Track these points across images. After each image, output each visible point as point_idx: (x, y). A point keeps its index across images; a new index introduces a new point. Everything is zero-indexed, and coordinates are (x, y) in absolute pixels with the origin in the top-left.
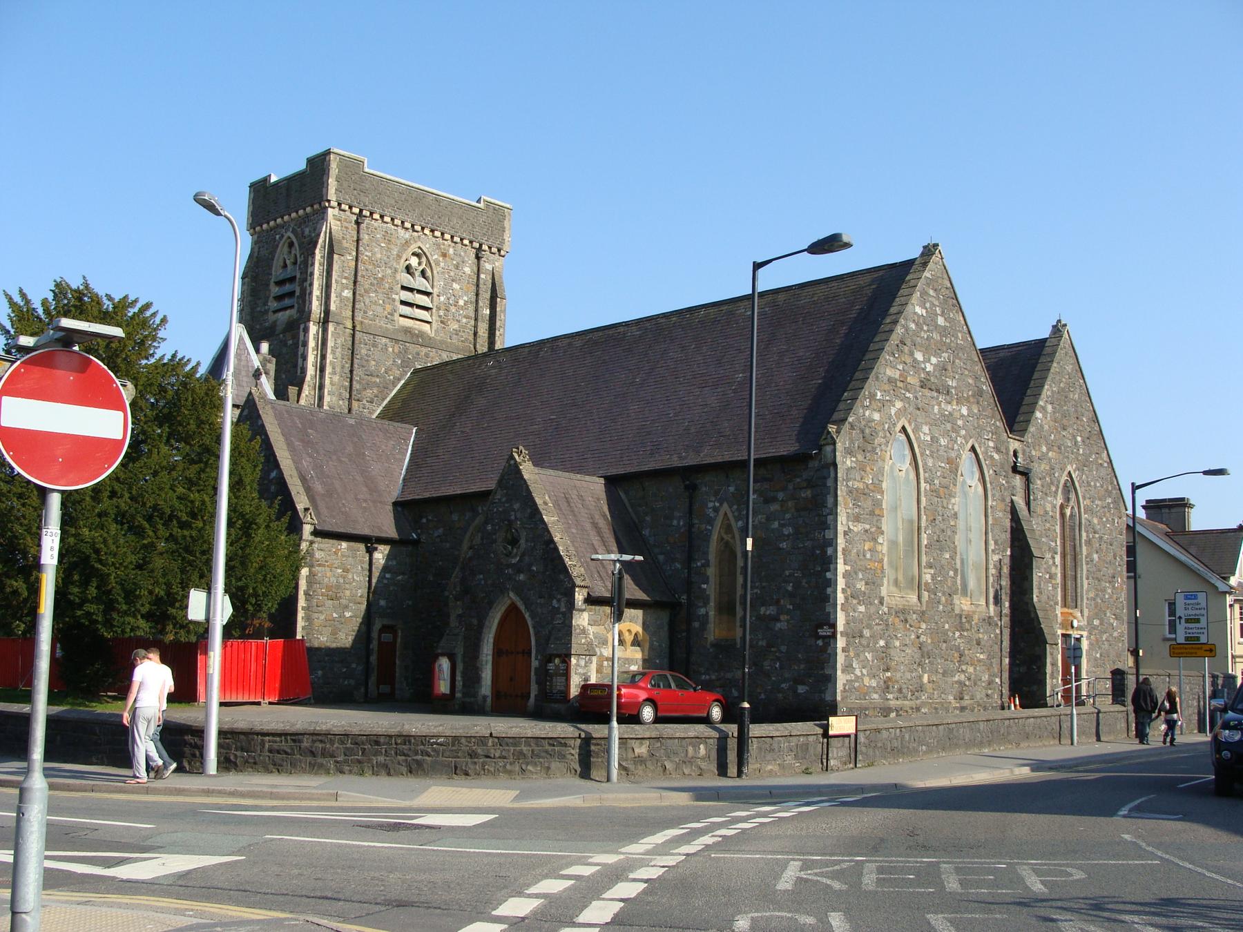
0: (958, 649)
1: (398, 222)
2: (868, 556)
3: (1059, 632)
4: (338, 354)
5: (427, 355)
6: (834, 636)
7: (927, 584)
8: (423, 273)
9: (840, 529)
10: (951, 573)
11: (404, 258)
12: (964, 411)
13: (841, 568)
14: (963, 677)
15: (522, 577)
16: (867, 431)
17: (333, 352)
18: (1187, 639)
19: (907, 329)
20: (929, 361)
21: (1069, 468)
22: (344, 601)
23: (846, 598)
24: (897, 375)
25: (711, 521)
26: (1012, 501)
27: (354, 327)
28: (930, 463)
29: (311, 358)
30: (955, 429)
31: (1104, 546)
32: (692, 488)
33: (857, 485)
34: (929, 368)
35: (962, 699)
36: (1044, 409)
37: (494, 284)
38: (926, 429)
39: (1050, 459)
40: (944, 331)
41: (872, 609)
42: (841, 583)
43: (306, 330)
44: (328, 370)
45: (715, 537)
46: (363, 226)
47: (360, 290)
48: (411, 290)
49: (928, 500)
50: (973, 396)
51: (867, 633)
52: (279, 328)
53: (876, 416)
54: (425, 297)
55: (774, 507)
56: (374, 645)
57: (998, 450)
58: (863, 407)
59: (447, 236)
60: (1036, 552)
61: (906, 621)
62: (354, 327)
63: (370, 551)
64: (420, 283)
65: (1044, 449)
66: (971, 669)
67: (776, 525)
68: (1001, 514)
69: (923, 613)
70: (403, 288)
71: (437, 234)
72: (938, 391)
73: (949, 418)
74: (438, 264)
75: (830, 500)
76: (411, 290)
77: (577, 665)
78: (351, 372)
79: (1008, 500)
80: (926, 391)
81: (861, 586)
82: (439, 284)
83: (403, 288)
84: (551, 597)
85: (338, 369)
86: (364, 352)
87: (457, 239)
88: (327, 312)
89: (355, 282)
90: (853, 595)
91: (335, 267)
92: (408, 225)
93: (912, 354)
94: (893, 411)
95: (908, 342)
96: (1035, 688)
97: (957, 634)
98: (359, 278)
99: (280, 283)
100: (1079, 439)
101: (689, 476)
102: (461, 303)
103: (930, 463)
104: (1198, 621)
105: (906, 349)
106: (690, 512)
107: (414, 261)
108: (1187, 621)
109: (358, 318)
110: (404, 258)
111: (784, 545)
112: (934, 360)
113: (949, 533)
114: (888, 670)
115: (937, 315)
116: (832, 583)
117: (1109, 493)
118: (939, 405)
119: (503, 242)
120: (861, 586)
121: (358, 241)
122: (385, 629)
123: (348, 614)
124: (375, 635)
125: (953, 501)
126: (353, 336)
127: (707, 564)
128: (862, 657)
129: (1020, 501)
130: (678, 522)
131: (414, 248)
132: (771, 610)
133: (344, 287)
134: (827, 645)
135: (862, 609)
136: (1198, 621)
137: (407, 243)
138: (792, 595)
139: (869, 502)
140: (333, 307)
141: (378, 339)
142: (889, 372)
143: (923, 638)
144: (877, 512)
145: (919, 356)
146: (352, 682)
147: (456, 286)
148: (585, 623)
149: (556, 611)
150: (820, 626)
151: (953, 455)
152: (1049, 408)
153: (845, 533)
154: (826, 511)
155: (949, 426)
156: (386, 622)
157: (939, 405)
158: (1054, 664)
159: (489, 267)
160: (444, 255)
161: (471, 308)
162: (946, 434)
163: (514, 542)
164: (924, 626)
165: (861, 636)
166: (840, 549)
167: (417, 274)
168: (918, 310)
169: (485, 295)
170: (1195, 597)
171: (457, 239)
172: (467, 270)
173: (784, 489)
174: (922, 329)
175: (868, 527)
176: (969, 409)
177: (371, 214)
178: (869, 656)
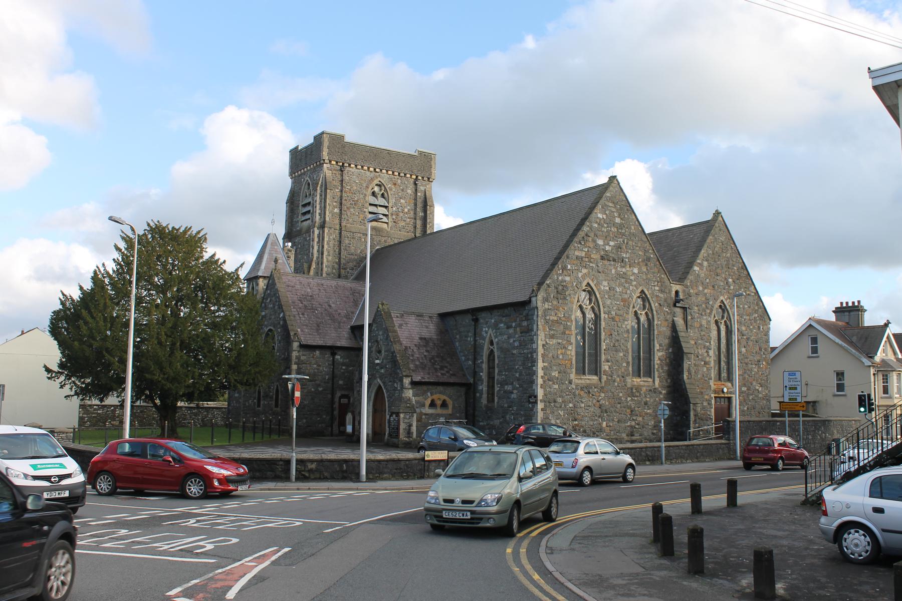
0: (629, 407)
1: (366, 168)
2: (561, 357)
3: (713, 395)
4: (332, 245)
5: (385, 241)
6: (536, 402)
7: (605, 371)
8: (383, 195)
9: (540, 343)
10: (625, 364)
11: (370, 187)
12: (636, 271)
13: (540, 364)
14: (633, 423)
15: (382, 371)
16: (560, 288)
17: (328, 244)
18: (790, 399)
19: (591, 228)
20: (608, 244)
21: (722, 298)
22: (318, 382)
23: (544, 382)
24: (583, 254)
25: (484, 339)
26: (673, 321)
27: (341, 229)
28: (608, 302)
29: (316, 248)
30: (629, 282)
31: (750, 343)
32: (476, 320)
33: (552, 318)
34: (607, 248)
35: (632, 435)
36: (701, 265)
37: (425, 198)
38: (605, 283)
39: (706, 294)
40: (621, 226)
41: (564, 387)
42: (540, 373)
43: (313, 232)
44: (325, 253)
45: (486, 347)
46: (345, 172)
47: (344, 208)
48: (376, 205)
49: (607, 324)
50: (643, 261)
51: (560, 400)
52: (304, 231)
53: (568, 279)
54: (384, 209)
55: (511, 331)
56: (336, 405)
57: (661, 291)
58: (558, 274)
59: (396, 174)
60: (685, 350)
61: (589, 392)
62: (341, 229)
63: (333, 354)
64: (381, 201)
65: (701, 288)
66: (641, 419)
67: (511, 341)
68: (665, 329)
69: (602, 387)
70: (371, 205)
71: (390, 172)
72: (614, 260)
73: (624, 276)
74: (391, 190)
75: (535, 327)
76: (376, 205)
77: (404, 418)
78: (340, 254)
79: (671, 320)
80: (606, 262)
81: (555, 374)
82: (392, 201)
83: (371, 205)
84: (394, 382)
85: (331, 252)
86: (347, 242)
87: (402, 175)
88: (324, 222)
89: (341, 204)
90: (548, 379)
91: (328, 196)
92: (372, 169)
93: (594, 241)
94: (580, 275)
95: (592, 235)
96: (684, 429)
97: (629, 399)
98: (343, 201)
99: (304, 206)
100: (730, 280)
101: (475, 313)
102: (406, 210)
103: (608, 302)
104: (796, 389)
105: (590, 239)
106: (475, 334)
107: (376, 189)
108: (790, 389)
109: (343, 224)
110: (370, 187)
111: (515, 352)
112: (612, 243)
113: (623, 341)
114: (576, 420)
115: (615, 217)
116: (534, 373)
117: (756, 312)
118: (616, 268)
119: (431, 174)
120: (555, 374)
121: (342, 181)
122: (343, 396)
123: (320, 389)
124: (337, 399)
125: (626, 323)
126: (340, 233)
127: (482, 362)
128: (556, 413)
129: (679, 321)
130: (470, 339)
131: (376, 182)
132: (509, 388)
133: (335, 207)
134: (533, 407)
135: (556, 386)
136: (796, 389)
137: (372, 179)
138: (518, 379)
139: (562, 327)
140: (327, 219)
141: (355, 235)
142: (577, 253)
143: (602, 402)
144: (567, 332)
145: (600, 242)
146: (323, 425)
147: (402, 201)
148: (411, 395)
149: (396, 389)
150: (530, 397)
151: (626, 296)
152: (705, 263)
153: (543, 345)
154: (533, 333)
155: (623, 280)
156: (344, 393)
157: (616, 268)
158: (305, 452)
159: (422, 188)
160: (395, 184)
161: (412, 213)
162: (621, 285)
163: (380, 352)
164: (603, 395)
165: (555, 402)
166: (540, 354)
167: (379, 196)
168: (600, 216)
169: (420, 205)
170: (795, 374)
171: (402, 175)
172: (409, 191)
173: (515, 321)
174: (603, 226)
175: (560, 341)
176: (640, 269)
177: (350, 165)
178: (562, 413)
